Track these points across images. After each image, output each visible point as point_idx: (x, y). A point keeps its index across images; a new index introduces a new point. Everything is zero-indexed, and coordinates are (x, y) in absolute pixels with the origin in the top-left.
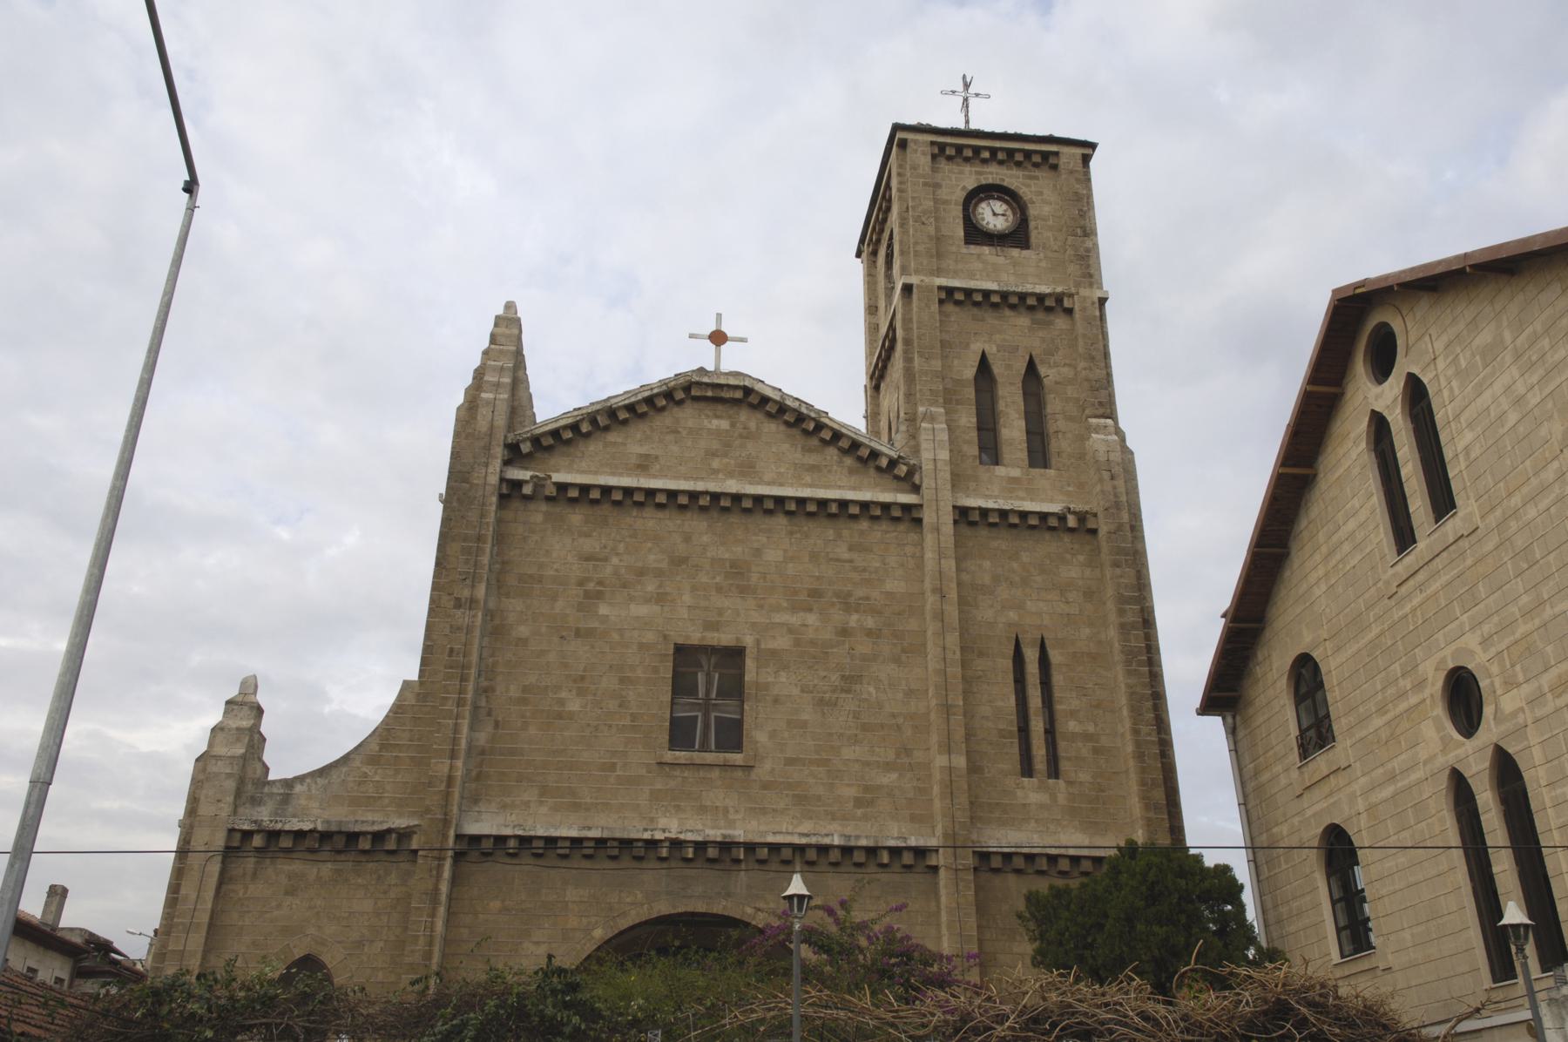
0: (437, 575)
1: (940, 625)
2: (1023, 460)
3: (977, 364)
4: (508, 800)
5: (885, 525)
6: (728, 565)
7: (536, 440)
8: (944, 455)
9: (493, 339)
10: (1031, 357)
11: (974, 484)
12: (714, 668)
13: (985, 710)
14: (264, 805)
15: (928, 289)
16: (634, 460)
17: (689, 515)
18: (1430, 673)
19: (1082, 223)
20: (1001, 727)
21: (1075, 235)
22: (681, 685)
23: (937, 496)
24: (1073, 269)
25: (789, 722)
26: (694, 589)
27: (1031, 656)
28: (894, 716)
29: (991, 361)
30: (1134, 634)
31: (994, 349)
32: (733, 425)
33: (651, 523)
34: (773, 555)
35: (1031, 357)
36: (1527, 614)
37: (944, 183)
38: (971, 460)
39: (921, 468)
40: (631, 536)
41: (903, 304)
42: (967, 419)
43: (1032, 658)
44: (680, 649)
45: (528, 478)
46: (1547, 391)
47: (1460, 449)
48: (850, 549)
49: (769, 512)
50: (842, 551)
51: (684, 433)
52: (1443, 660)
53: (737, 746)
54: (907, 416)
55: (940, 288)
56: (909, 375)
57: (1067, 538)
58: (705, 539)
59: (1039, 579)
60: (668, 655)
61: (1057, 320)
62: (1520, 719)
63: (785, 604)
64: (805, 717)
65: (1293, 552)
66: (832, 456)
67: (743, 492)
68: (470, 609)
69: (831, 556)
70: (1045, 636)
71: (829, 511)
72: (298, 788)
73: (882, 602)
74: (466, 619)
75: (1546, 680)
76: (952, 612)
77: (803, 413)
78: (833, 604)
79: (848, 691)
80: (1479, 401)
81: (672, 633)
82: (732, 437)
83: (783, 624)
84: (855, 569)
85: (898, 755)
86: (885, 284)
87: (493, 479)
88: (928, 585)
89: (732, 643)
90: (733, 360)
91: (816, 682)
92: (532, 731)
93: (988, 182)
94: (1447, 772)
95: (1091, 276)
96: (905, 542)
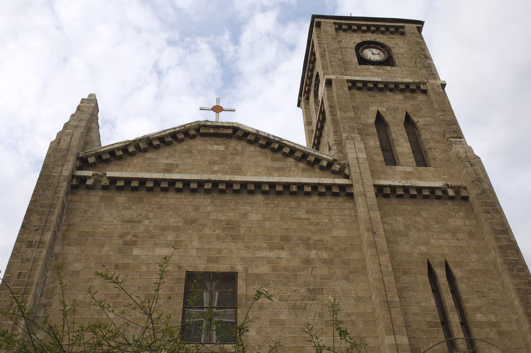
0: (21, 233)
1: (375, 250)
2: (412, 163)
3: (375, 116)
5: (328, 199)
6: (224, 223)
7: (99, 157)
8: (363, 155)
9: (79, 108)
10: (407, 113)
11: (384, 176)
12: (215, 288)
13: (415, 309)
15: (342, 81)
16: (162, 167)
17: (198, 195)
19: (424, 53)
20: (428, 320)
23: (361, 177)
24: (424, 72)
25: (271, 322)
26: (200, 238)
27: (441, 273)
28: (349, 315)
29: (383, 115)
30: (510, 253)
31: (384, 110)
33: (172, 201)
34: (254, 217)
35: (407, 113)
37: (343, 41)
38: (380, 163)
39: (349, 165)
40: (158, 208)
41: (327, 90)
42: (374, 142)
43: (442, 274)
44: (190, 276)
45: (91, 175)
48: (308, 212)
49: (251, 192)
50: (302, 214)
51: (195, 152)
54: (336, 142)
55: (348, 81)
56: (335, 122)
57: (449, 203)
59: (435, 226)
60: (181, 279)
61: (419, 96)
63: (265, 246)
64: (283, 317)
66: (291, 163)
67: (233, 180)
68: (38, 248)
69: (294, 217)
70: (448, 260)
71: (291, 190)
73: (332, 243)
74: (34, 254)
76: (382, 242)
77: (271, 139)
78: (298, 245)
79: (313, 299)
81: (184, 265)
82: (227, 154)
83: (264, 258)
84: (312, 224)
86: (315, 107)
87: (66, 172)
88: (362, 228)
89: (229, 270)
90: (224, 118)
91: (289, 294)
93: (367, 40)
95: (434, 75)
96: (343, 207)
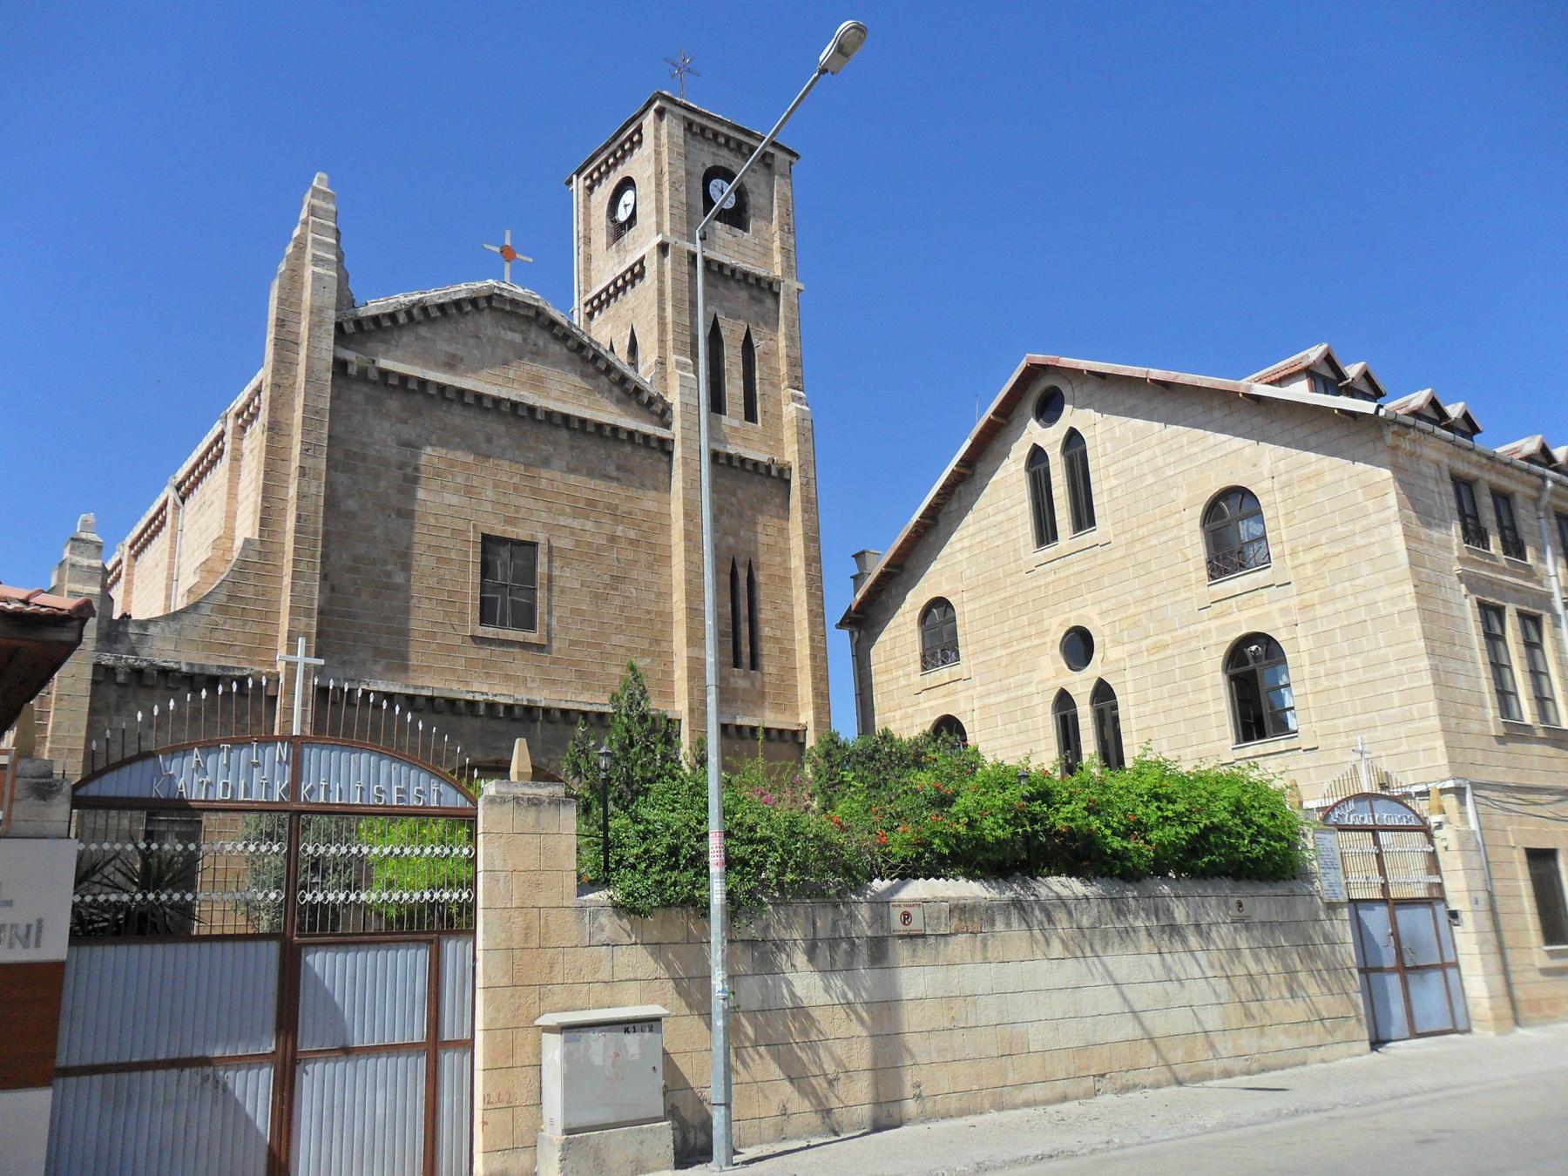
4: (346, 658)
14: (120, 643)
17: (490, 417)
18: (1054, 627)
21: (783, 230)
22: (486, 569)
26: (495, 486)
27: (743, 574)
32: (525, 340)
36: (1137, 602)
40: (441, 429)
46: (1179, 470)
47: (1105, 488)
51: (485, 340)
52: (1068, 620)
53: (531, 626)
58: (504, 442)
62: (1122, 665)
65: (941, 525)
72: (152, 630)
75: (1144, 644)
79: (616, 589)
80: (1126, 462)
85: (650, 644)
92: (364, 597)
94: (1057, 690)
